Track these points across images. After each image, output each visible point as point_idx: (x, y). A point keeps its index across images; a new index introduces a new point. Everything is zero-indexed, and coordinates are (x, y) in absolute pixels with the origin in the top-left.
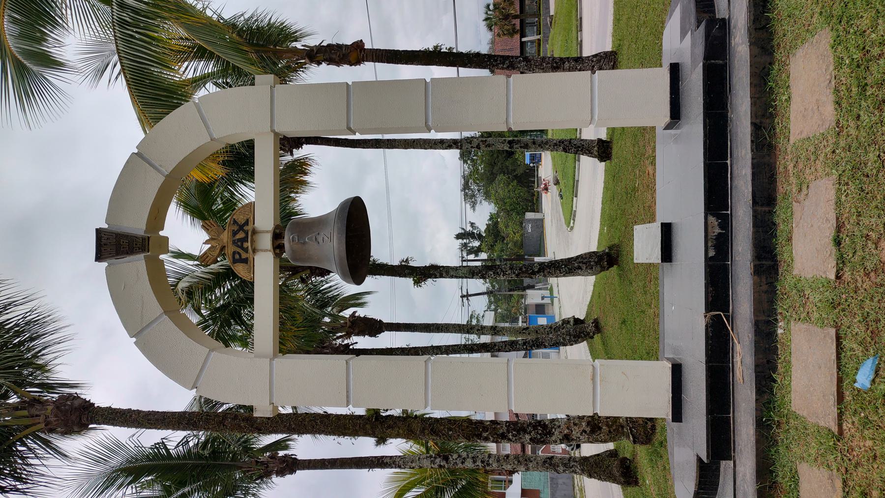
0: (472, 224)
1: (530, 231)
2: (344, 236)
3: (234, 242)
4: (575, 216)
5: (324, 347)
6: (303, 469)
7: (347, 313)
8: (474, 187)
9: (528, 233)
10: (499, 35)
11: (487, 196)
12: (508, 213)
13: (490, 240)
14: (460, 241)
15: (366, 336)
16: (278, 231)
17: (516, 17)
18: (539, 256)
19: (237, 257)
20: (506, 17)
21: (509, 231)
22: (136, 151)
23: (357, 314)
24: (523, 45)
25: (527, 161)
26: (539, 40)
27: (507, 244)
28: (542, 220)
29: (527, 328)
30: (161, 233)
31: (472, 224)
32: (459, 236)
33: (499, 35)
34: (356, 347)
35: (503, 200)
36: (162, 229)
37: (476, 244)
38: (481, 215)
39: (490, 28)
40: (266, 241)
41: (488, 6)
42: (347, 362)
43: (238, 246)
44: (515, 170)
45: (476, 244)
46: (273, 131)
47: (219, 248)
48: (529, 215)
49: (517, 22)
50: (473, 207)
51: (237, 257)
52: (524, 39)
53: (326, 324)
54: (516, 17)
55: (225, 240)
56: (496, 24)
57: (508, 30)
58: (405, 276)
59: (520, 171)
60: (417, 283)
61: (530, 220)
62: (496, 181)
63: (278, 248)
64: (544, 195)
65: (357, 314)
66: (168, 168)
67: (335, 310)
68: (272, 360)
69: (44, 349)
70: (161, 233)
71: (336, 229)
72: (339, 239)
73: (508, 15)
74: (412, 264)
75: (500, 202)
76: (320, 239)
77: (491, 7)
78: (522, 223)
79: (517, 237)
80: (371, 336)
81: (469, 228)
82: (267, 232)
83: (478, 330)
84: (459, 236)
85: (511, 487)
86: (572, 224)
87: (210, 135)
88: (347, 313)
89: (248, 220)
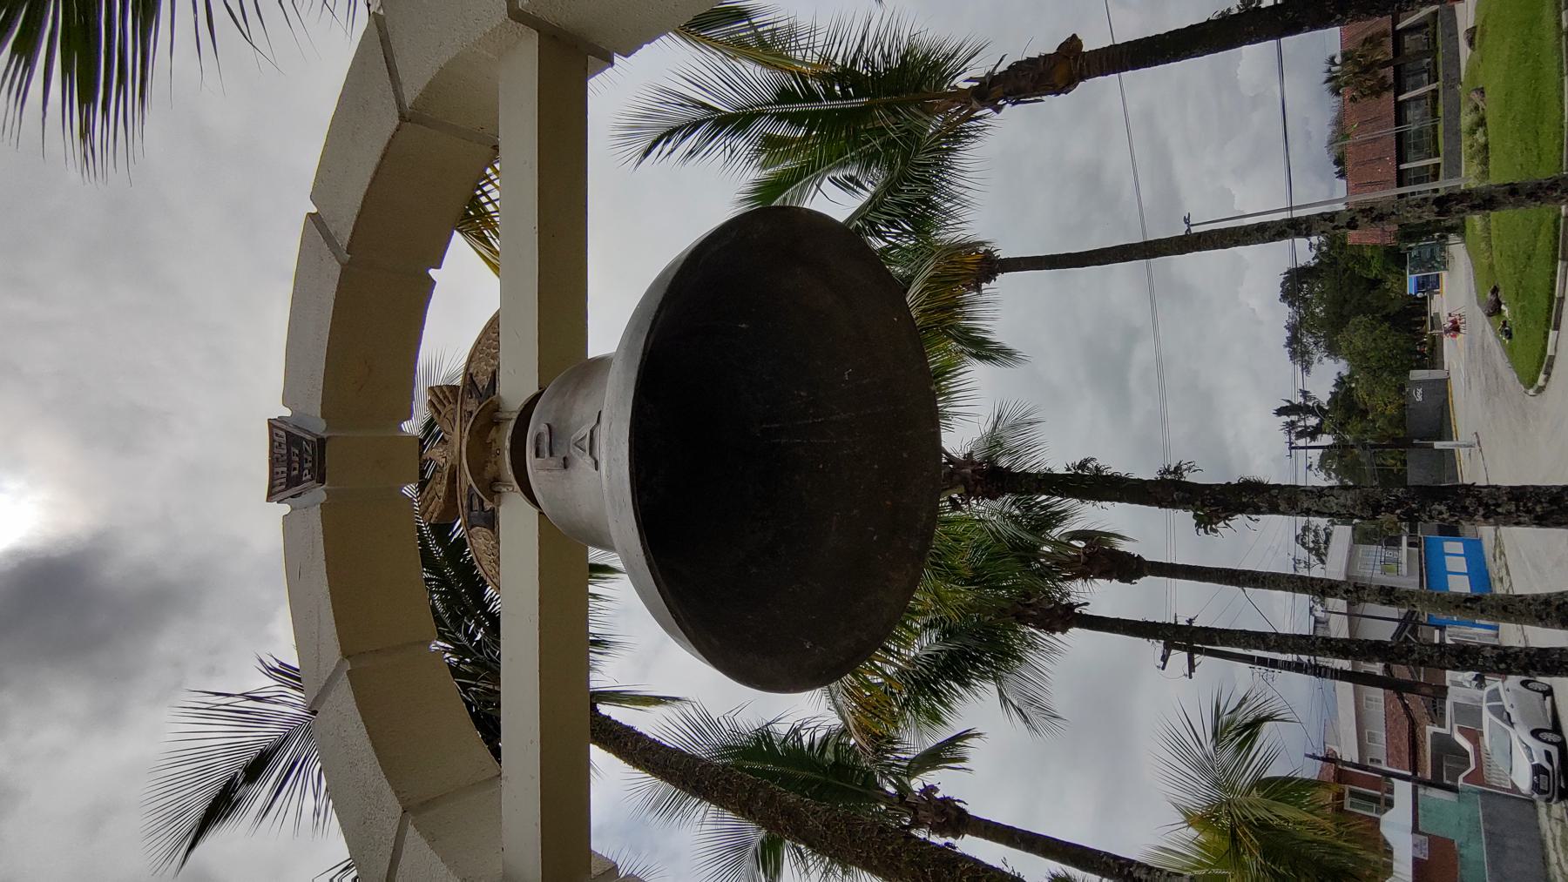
0: (1305, 394)
1: (1419, 398)
2: (633, 375)
4: (1550, 366)
5: (1029, 606)
6: (976, 834)
8: (1308, 340)
9: (1415, 402)
10: (1353, 99)
11: (1333, 350)
12: (1374, 373)
13: (1338, 416)
14: (1285, 419)
15: (1115, 581)
17: (1386, 64)
18: (1439, 439)
20: (1368, 69)
21: (1381, 403)
24: (1400, 108)
25: (1411, 289)
26: (1435, 91)
27: (1373, 421)
28: (1444, 382)
29: (1478, 599)
31: (1305, 394)
32: (1281, 412)
33: (1353, 99)
35: (1362, 354)
37: (1313, 421)
38: (1324, 377)
39: (1336, 91)
41: (1332, 61)
44: (1385, 307)
45: (1313, 421)
48: (1417, 375)
49: (1389, 72)
50: (1306, 368)
52: (1401, 98)
53: (1046, 555)
54: (1386, 64)
56: (1347, 84)
57: (1370, 88)
58: (1173, 505)
59: (1394, 308)
60: (1206, 522)
61: (1419, 383)
62: (1350, 326)
64: (1447, 340)
69: (275, 670)
73: (1373, 64)
74: (1189, 477)
75: (1359, 360)
77: (1338, 60)
78: (1402, 388)
79: (1391, 410)
80: (1122, 580)
81: (1299, 400)
83: (1347, 591)
84: (1281, 412)
85: (1390, 812)
86: (1541, 382)
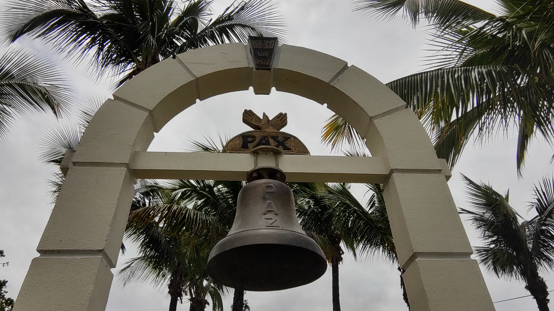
3: (264, 138)
5: (181, 277)
7: (208, 298)
16: (278, 175)
19: (250, 139)
22: (349, 65)
23: (207, 305)
30: (273, 89)
34: (179, 302)
36: (277, 90)
40: (266, 162)
42: (100, 251)
43: (261, 141)
46: (392, 171)
47: (260, 125)
51: (250, 139)
55: (267, 130)
63: (258, 174)
65: (207, 305)
66: (338, 85)
67: (212, 289)
68: (127, 165)
70: (273, 89)
71: (284, 232)
72: (270, 235)
76: (269, 216)
82: (277, 165)
87: (376, 117)
88: (208, 298)
89: (290, 149)
